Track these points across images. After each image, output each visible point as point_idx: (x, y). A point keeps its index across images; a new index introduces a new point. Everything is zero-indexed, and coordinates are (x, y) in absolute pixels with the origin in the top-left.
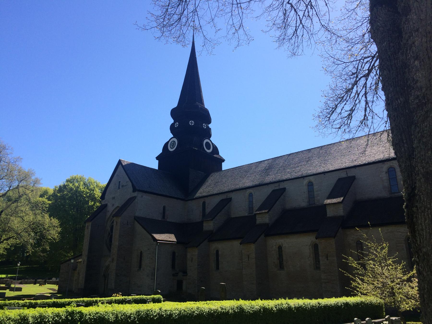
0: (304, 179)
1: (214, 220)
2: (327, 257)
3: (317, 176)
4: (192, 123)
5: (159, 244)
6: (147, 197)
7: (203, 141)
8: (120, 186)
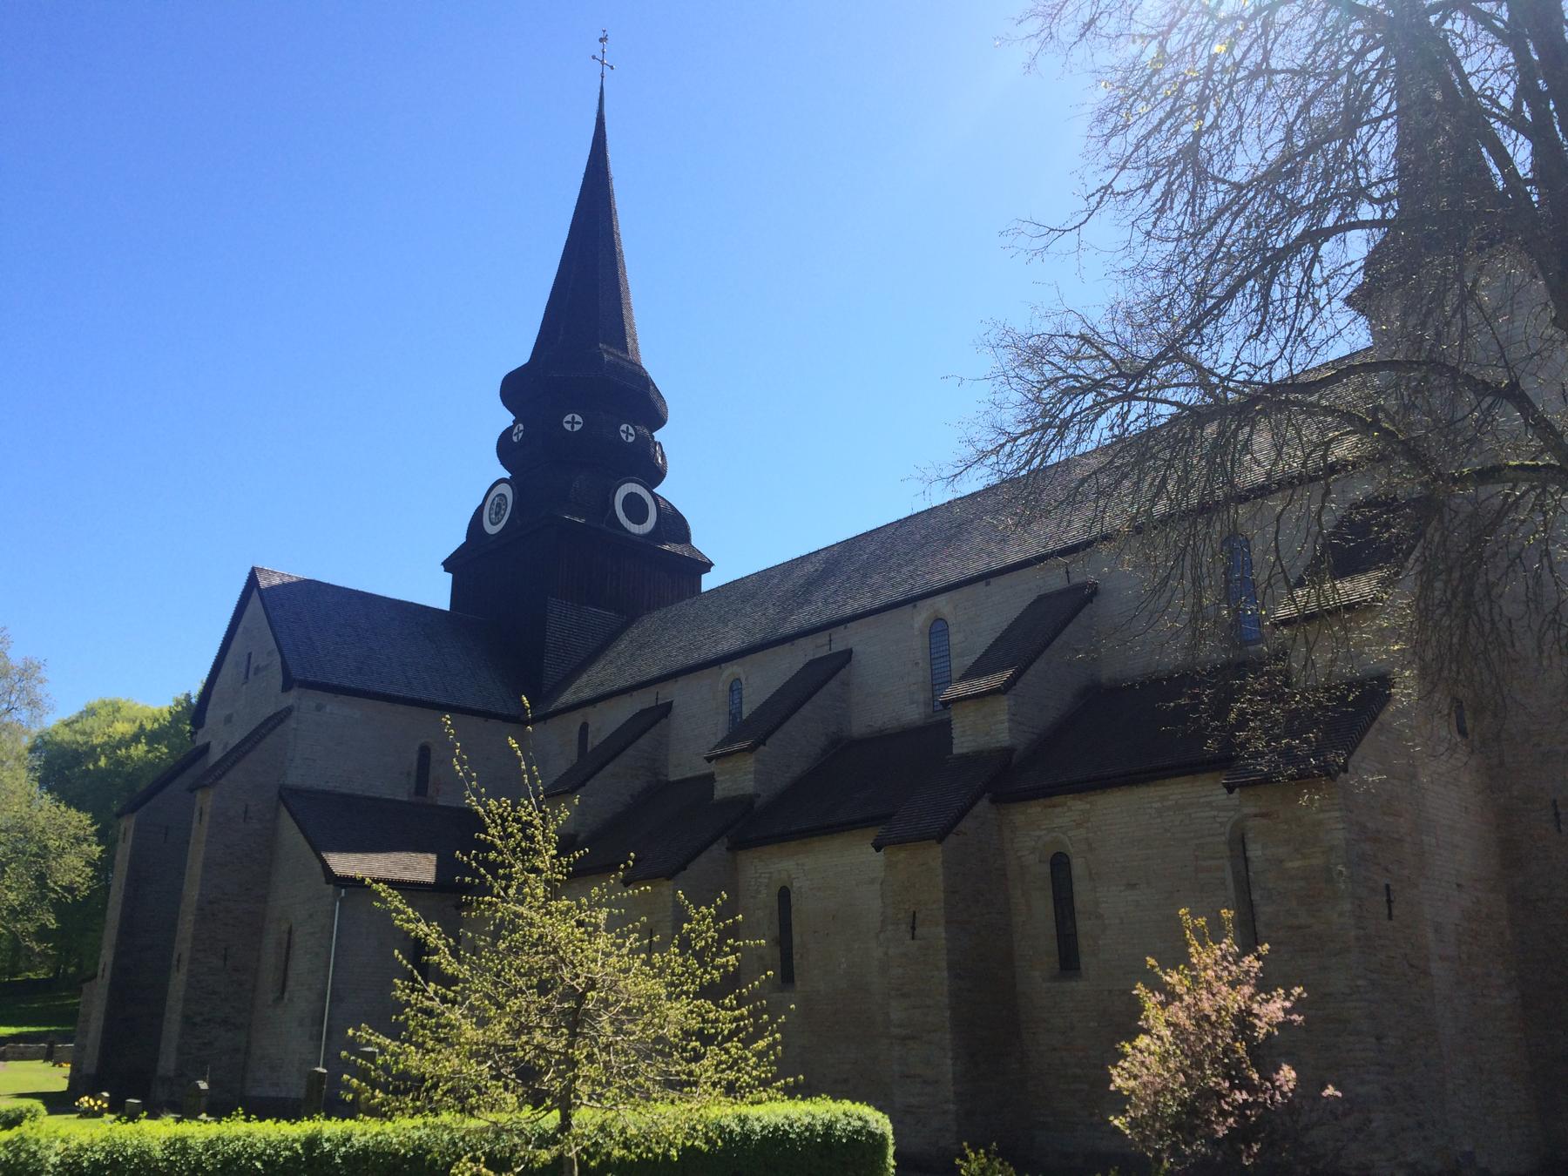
2: (913, 928)
3: (966, 590)
4: (573, 422)
5: (343, 894)
6: (339, 710)
7: (610, 496)
8: (250, 670)
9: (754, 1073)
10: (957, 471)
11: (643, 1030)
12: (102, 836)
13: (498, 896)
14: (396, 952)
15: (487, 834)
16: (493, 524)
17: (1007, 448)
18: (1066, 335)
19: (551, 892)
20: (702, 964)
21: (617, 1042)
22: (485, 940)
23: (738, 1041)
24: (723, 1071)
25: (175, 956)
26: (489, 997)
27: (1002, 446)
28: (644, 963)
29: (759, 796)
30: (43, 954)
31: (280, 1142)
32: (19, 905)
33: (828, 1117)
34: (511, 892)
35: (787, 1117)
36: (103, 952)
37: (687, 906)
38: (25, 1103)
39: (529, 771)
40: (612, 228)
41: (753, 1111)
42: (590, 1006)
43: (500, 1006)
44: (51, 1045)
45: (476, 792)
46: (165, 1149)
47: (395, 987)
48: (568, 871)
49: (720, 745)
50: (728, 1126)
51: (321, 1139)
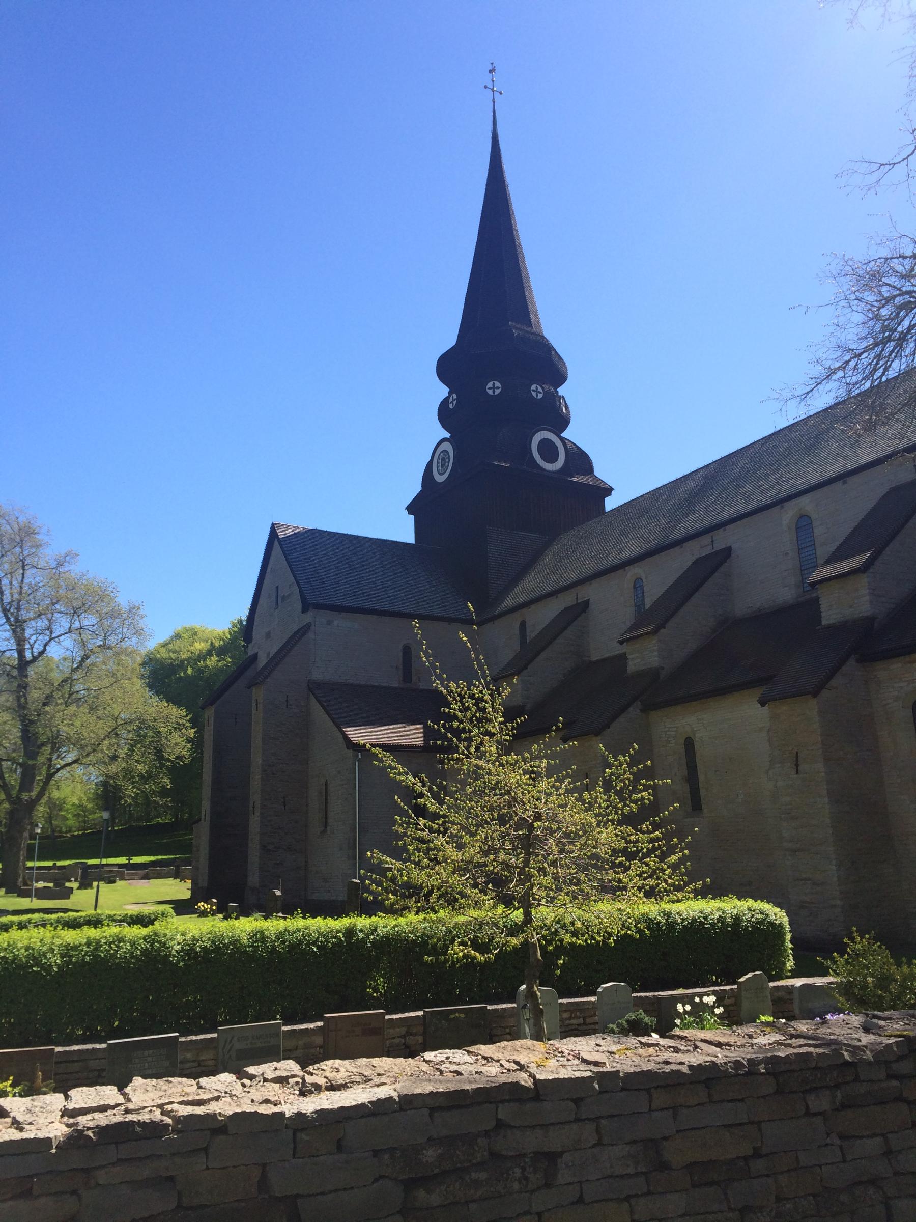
0: (782, 507)
1: (525, 672)
2: (797, 765)
4: (494, 388)
5: (360, 756)
6: (342, 623)
8: (279, 600)
9: (670, 881)
10: (809, 389)
11: (580, 849)
12: (194, 723)
13: (463, 753)
14: (396, 797)
15: (450, 708)
16: (441, 474)
17: (852, 363)
18: (900, 256)
19: (501, 750)
20: (622, 799)
21: (561, 858)
22: (456, 787)
23: (655, 857)
24: (645, 879)
25: (251, 805)
26: (463, 828)
27: (847, 362)
28: (577, 800)
29: (663, 668)
30: (165, 806)
31: (328, 933)
32: (145, 773)
33: (735, 912)
34: (472, 750)
35: (702, 912)
36: (203, 802)
37: (607, 756)
38: (161, 908)
39: (478, 661)
40: (512, 226)
41: (675, 908)
42: (539, 833)
43: (473, 835)
44: (178, 867)
45: (439, 677)
46: (251, 938)
47: (395, 823)
48: (513, 733)
49: (630, 630)
50: (655, 919)
51: (356, 929)
